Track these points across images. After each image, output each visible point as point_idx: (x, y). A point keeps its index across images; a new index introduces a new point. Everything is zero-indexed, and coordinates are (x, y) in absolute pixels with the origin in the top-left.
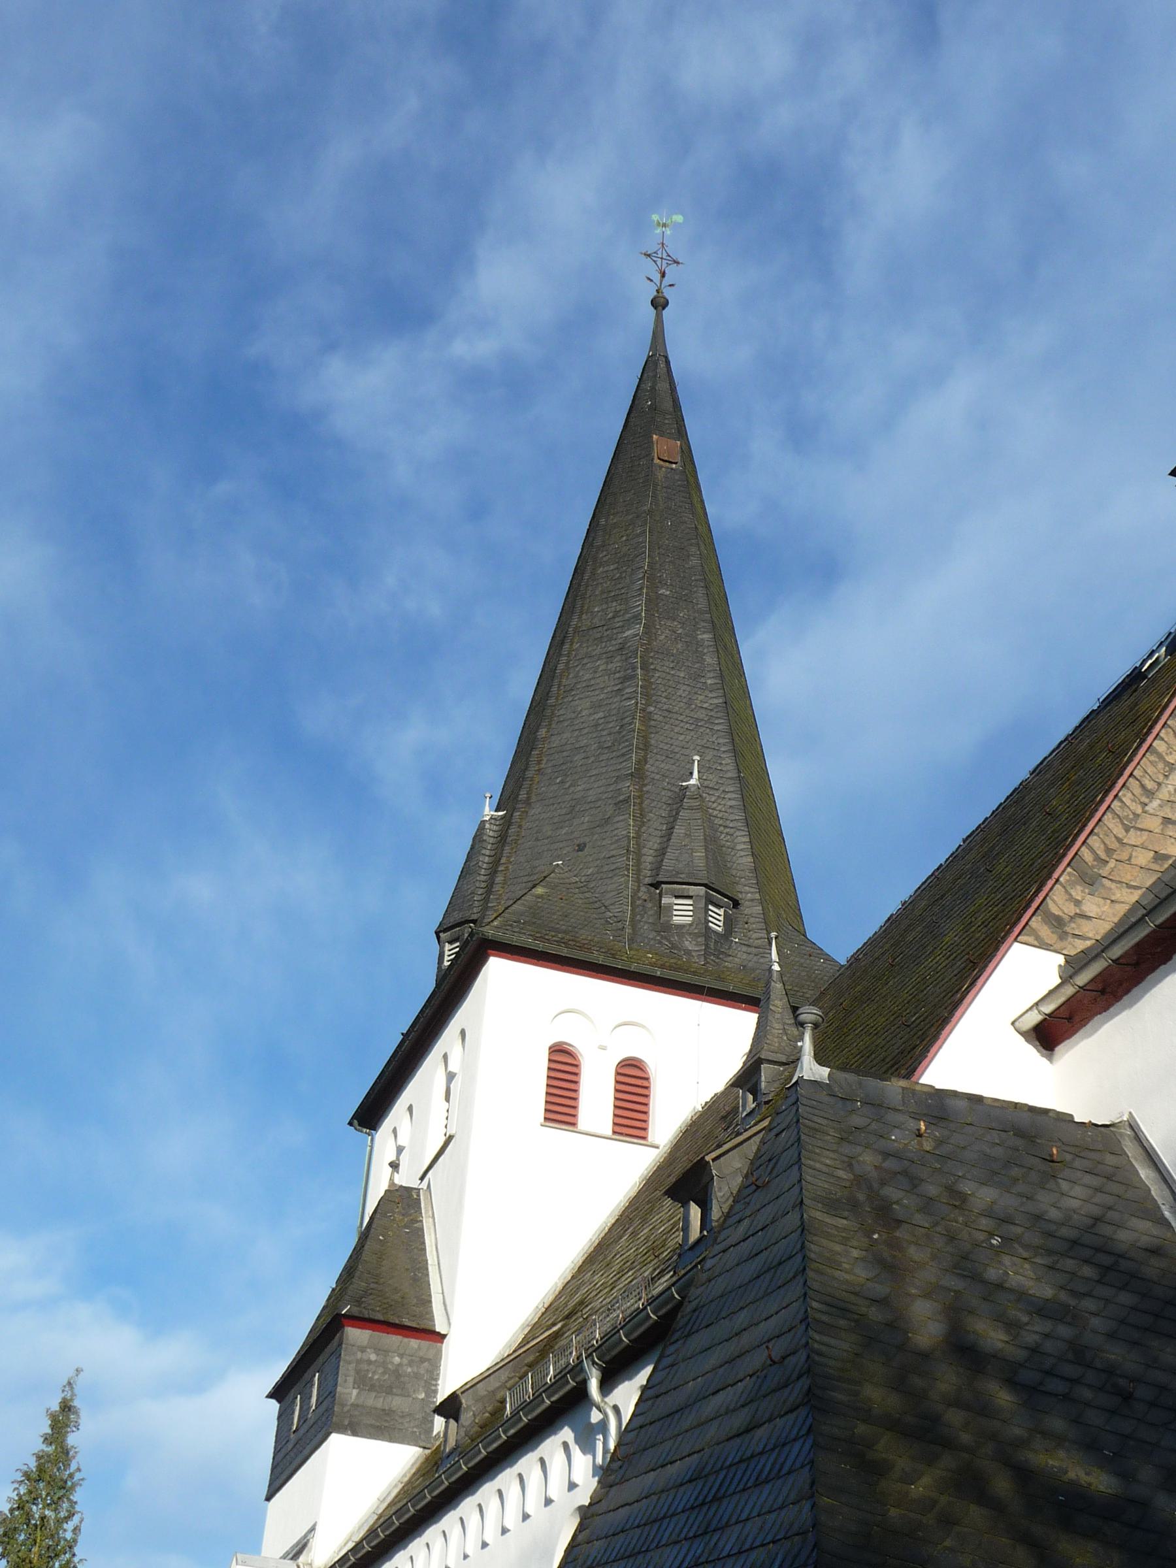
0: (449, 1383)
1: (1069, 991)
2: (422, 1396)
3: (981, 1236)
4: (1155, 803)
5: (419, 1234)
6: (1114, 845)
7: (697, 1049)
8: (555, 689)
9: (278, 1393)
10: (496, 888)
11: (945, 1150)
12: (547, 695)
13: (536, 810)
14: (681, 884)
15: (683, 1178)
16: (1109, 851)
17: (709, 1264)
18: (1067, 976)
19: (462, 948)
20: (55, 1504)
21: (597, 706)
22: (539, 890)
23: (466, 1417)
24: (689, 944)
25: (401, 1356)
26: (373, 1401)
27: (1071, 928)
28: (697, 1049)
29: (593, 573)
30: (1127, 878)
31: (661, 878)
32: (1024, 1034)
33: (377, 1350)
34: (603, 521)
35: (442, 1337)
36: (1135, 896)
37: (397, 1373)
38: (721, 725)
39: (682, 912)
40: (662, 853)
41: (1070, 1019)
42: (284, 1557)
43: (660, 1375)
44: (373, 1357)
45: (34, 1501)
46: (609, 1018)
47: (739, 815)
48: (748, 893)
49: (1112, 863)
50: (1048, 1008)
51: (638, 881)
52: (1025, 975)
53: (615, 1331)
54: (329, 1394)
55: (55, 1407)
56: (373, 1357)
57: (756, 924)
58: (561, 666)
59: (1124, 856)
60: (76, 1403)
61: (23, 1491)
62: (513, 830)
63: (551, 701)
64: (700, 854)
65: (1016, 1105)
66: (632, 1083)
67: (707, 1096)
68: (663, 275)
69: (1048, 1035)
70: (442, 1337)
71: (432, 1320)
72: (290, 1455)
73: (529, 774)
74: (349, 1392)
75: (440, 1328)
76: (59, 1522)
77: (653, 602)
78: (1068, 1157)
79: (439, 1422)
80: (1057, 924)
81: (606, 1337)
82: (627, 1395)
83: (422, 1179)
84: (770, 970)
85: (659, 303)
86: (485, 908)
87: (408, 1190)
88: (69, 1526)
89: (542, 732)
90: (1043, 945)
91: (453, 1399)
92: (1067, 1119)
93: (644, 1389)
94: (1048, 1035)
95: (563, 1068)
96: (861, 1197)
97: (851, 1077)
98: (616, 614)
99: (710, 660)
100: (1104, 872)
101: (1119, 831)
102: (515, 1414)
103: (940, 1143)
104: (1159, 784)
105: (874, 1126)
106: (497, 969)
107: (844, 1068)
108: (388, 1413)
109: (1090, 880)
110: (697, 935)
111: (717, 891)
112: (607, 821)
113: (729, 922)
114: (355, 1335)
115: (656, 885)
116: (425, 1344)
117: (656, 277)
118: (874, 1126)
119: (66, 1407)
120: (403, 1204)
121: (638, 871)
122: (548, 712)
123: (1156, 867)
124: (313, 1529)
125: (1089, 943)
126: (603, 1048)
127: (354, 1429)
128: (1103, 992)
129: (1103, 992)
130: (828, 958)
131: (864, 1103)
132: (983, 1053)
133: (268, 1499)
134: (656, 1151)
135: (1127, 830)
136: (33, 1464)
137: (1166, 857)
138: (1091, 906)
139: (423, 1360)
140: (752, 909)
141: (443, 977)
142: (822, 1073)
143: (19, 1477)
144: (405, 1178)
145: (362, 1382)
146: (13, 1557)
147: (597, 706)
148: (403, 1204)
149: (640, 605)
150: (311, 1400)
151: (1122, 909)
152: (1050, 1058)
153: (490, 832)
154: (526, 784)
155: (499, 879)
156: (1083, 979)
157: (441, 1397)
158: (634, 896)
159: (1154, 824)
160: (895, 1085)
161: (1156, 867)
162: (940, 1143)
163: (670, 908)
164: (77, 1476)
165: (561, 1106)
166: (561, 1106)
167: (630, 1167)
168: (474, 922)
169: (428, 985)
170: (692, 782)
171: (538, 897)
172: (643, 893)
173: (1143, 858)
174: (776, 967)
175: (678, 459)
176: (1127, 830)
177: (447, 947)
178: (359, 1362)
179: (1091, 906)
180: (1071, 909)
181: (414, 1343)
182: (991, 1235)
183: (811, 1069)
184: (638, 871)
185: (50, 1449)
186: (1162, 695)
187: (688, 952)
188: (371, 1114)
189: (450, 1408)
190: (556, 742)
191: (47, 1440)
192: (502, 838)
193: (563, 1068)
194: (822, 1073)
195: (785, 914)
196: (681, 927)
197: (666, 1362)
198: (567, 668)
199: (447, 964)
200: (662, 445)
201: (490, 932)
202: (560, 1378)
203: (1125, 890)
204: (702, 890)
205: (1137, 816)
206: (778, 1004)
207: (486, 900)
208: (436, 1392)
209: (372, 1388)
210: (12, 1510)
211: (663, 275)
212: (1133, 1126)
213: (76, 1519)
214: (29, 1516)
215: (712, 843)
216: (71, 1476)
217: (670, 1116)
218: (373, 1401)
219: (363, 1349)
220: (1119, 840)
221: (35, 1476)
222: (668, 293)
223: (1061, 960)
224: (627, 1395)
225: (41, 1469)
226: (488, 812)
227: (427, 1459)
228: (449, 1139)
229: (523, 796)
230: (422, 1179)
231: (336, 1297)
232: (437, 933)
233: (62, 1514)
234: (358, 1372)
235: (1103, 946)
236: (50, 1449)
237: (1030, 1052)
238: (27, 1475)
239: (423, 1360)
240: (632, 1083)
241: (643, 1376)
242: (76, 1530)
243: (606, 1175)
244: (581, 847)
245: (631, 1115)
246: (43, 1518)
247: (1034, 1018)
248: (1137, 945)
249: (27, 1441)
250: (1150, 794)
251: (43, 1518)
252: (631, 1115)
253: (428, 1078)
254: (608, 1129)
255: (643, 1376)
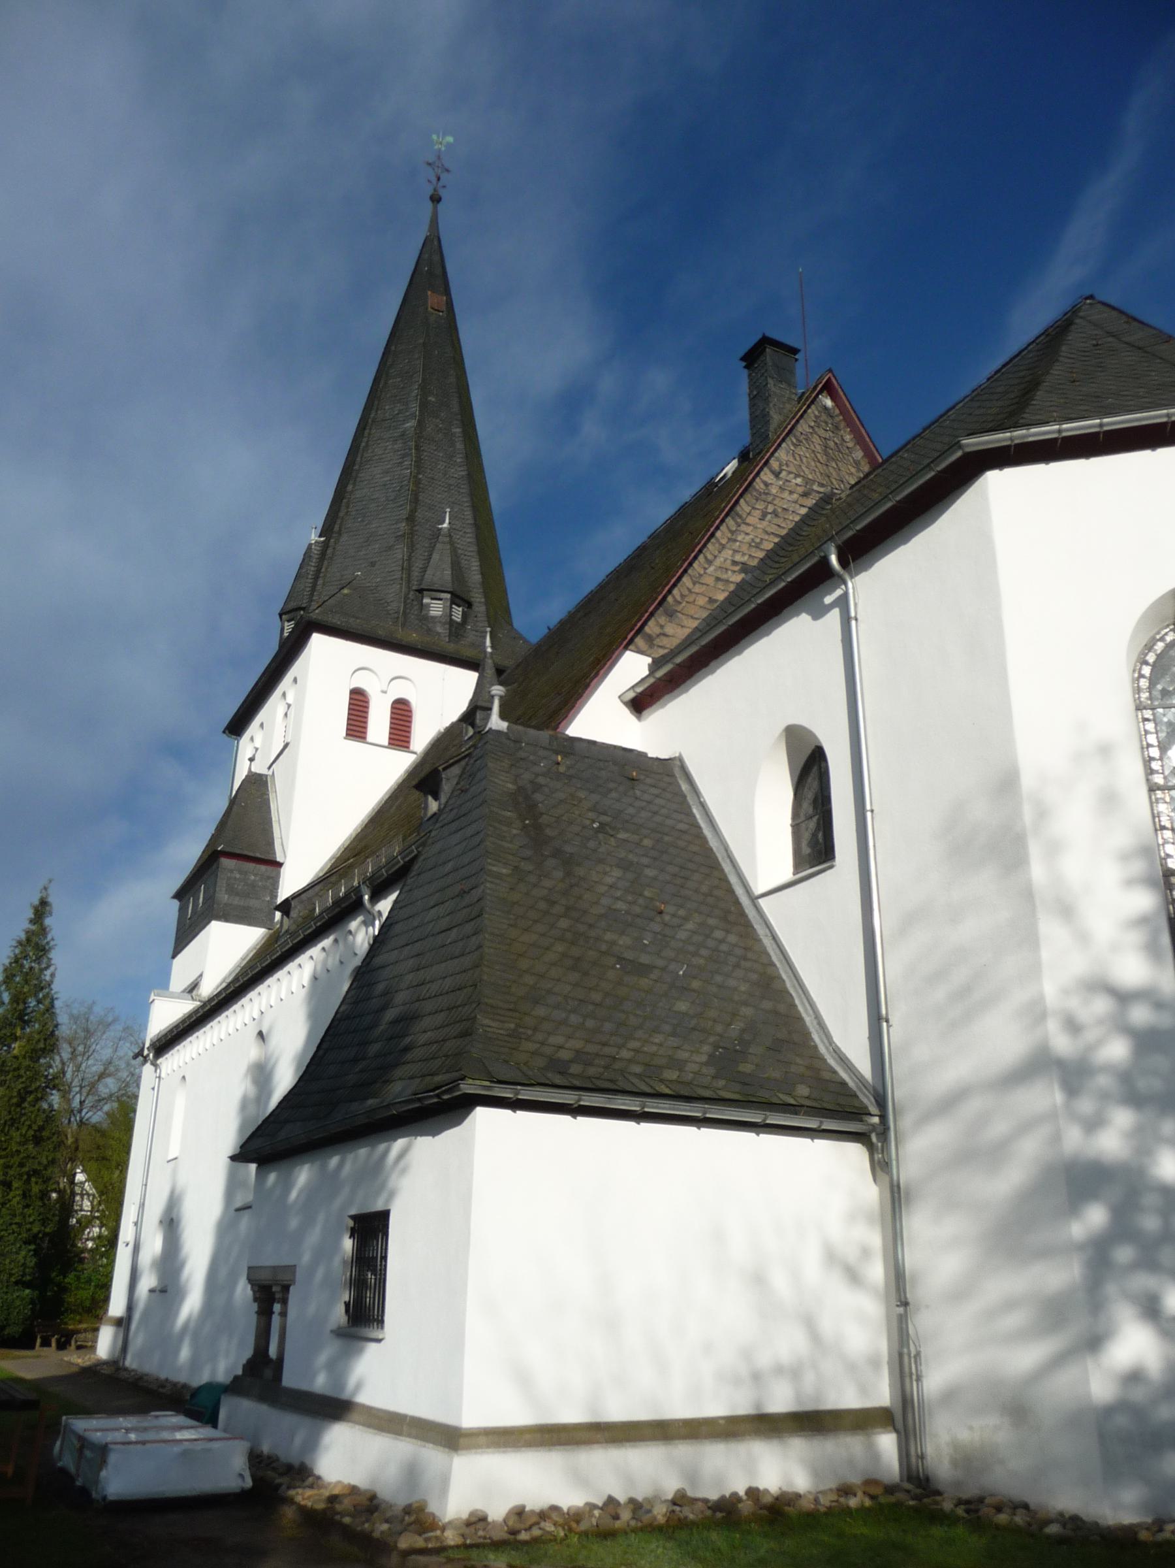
0: (286, 890)
1: (652, 680)
2: (268, 899)
3: (588, 822)
4: (712, 568)
5: (266, 803)
6: (686, 592)
7: (442, 694)
8: (358, 459)
9: (180, 895)
10: (318, 588)
11: (572, 772)
12: (354, 463)
13: (344, 538)
14: (435, 592)
15: (424, 780)
16: (682, 596)
17: (433, 834)
18: (654, 667)
19: (296, 625)
20: (38, 959)
21: (387, 472)
22: (346, 591)
23: (294, 914)
24: (439, 629)
25: (255, 875)
26: (236, 901)
27: (657, 642)
28: (442, 694)
29: (386, 383)
30: (692, 612)
31: (423, 587)
32: (626, 704)
33: (240, 872)
34: (393, 348)
35: (280, 865)
36: (695, 624)
37: (253, 886)
38: (465, 489)
39: (436, 608)
40: (424, 570)
41: (651, 696)
42: (183, 991)
43: (403, 896)
44: (238, 876)
45: (25, 958)
46: (388, 673)
47: (474, 548)
48: (477, 598)
49: (684, 604)
50: (639, 690)
51: (409, 588)
52: (631, 668)
53: (380, 868)
54: (210, 898)
55: (36, 902)
56: (238, 876)
57: (482, 617)
58: (363, 444)
59: (691, 599)
60: (50, 899)
61: (17, 951)
62: (329, 551)
63: (356, 467)
64: (449, 572)
65: (615, 747)
66: (401, 713)
67: (447, 724)
68: (439, 179)
69: (640, 703)
70: (280, 865)
71: (275, 853)
72: (186, 932)
73: (341, 514)
74: (223, 897)
75: (279, 859)
76: (42, 970)
77: (424, 405)
78: (642, 777)
79: (278, 915)
80: (650, 640)
81: (374, 874)
82: (385, 906)
83: (269, 768)
84: (485, 652)
85: (436, 199)
86: (311, 601)
87: (260, 775)
88: (48, 973)
89: (350, 488)
90: (639, 651)
91: (287, 902)
92: (643, 755)
93: (396, 902)
94: (640, 703)
95: (358, 702)
96: (521, 799)
97: (520, 728)
98: (400, 412)
99: (460, 446)
100: (679, 608)
101: (690, 585)
102: (321, 914)
103: (569, 768)
104: (715, 557)
105: (532, 758)
106: (317, 639)
107: (515, 723)
108: (248, 908)
109: (671, 615)
110: (445, 624)
111: (458, 598)
112: (390, 548)
113: (465, 616)
114: (225, 862)
115: (421, 591)
116: (269, 868)
117: (434, 180)
118: (532, 758)
119: (44, 903)
120: (257, 785)
121: (409, 581)
122: (354, 474)
123: (709, 606)
124: (201, 975)
125: (666, 651)
126: (385, 692)
127: (226, 917)
128: (670, 681)
129: (670, 681)
130: (526, 641)
131: (527, 744)
132: (601, 717)
133: (174, 957)
134: (414, 756)
135: (694, 583)
136: (23, 936)
137: (716, 601)
138: (670, 629)
139: (269, 878)
140: (480, 608)
141: (283, 643)
142: (503, 726)
143: (14, 943)
144: (259, 768)
145: (231, 890)
146: (12, 991)
147: (387, 472)
148: (257, 785)
149: (415, 407)
150: (202, 897)
151: (687, 631)
152: (639, 718)
153: (316, 551)
154: (339, 521)
155: (320, 582)
156: (660, 674)
157: (279, 901)
158: (406, 598)
159: (710, 581)
160: (545, 735)
161: (709, 606)
162: (569, 768)
163: (428, 605)
164: (52, 943)
165: (357, 727)
166: (357, 727)
167: (399, 764)
168: (304, 609)
169: (274, 647)
170: (445, 525)
171: (346, 595)
172: (411, 595)
173: (702, 601)
174: (489, 650)
175: (444, 308)
176: (694, 583)
177: (286, 624)
178: (229, 879)
179: (670, 629)
180: (657, 630)
181: (263, 868)
182: (594, 822)
183: (496, 722)
184: (409, 581)
185: (34, 928)
186: (722, 501)
187: (439, 634)
188: (238, 725)
189: (285, 907)
190: (358, 494)
191: (31, 921)
192: (323, 554)
193: (358, 702)
194: (503, 726)
195: (499, 615)
196: (434, 618)
197: (406, 888)
198: (367, 445)
199: (286, 634)
200: (434, 300)
201: (316, 614)
202: (347, 895)
203: (691, 621)
204: (448, 596)
205: (701, 575)
206: (490, 672)
207: (312, 595)
208: (276, 897)
209: (237, 894)
210: (11, 963)
211: (439, 179)
212: (680, 759)
213: (52, 969)
214: (22, 966)
215: (456, 567)
216: (48, 943)
217: (423, 736)
218: (236, 901)
219: (231, 871)
220: (690, 590)
221: (25, 942)
222: (442, 192)
223: (649, 660)
224: (385, 906)
225: (28, 940)
226: (314, 537)
227: (271, 936)
228: (286, 745)
229: (336, 528)
230: (269, 768)
231: (214, 839)
232: (281, 615)
233: (43, 966)
234: (228, 885)
235: (673, 653)
236: (34, 928)
237: (626, 713)
238: (20, 943)
239: (269, 878)
240: (401, 713)
241: (393, 897)
242: (53, 975)
243: (381, 770)
244: (373, 564)
245: (400, 735)
246: (31, 968)
247: (631, 695)
248: (691, 656)
249: (20, 926)
250: (710, 562)
251: (31, 968)
252: (400, 735)
253: (273, 710)
254: (386, 742)
255: (393, 897)
